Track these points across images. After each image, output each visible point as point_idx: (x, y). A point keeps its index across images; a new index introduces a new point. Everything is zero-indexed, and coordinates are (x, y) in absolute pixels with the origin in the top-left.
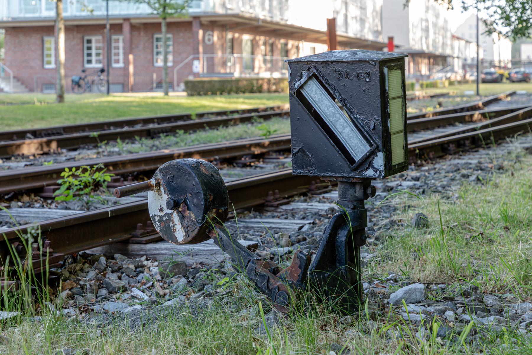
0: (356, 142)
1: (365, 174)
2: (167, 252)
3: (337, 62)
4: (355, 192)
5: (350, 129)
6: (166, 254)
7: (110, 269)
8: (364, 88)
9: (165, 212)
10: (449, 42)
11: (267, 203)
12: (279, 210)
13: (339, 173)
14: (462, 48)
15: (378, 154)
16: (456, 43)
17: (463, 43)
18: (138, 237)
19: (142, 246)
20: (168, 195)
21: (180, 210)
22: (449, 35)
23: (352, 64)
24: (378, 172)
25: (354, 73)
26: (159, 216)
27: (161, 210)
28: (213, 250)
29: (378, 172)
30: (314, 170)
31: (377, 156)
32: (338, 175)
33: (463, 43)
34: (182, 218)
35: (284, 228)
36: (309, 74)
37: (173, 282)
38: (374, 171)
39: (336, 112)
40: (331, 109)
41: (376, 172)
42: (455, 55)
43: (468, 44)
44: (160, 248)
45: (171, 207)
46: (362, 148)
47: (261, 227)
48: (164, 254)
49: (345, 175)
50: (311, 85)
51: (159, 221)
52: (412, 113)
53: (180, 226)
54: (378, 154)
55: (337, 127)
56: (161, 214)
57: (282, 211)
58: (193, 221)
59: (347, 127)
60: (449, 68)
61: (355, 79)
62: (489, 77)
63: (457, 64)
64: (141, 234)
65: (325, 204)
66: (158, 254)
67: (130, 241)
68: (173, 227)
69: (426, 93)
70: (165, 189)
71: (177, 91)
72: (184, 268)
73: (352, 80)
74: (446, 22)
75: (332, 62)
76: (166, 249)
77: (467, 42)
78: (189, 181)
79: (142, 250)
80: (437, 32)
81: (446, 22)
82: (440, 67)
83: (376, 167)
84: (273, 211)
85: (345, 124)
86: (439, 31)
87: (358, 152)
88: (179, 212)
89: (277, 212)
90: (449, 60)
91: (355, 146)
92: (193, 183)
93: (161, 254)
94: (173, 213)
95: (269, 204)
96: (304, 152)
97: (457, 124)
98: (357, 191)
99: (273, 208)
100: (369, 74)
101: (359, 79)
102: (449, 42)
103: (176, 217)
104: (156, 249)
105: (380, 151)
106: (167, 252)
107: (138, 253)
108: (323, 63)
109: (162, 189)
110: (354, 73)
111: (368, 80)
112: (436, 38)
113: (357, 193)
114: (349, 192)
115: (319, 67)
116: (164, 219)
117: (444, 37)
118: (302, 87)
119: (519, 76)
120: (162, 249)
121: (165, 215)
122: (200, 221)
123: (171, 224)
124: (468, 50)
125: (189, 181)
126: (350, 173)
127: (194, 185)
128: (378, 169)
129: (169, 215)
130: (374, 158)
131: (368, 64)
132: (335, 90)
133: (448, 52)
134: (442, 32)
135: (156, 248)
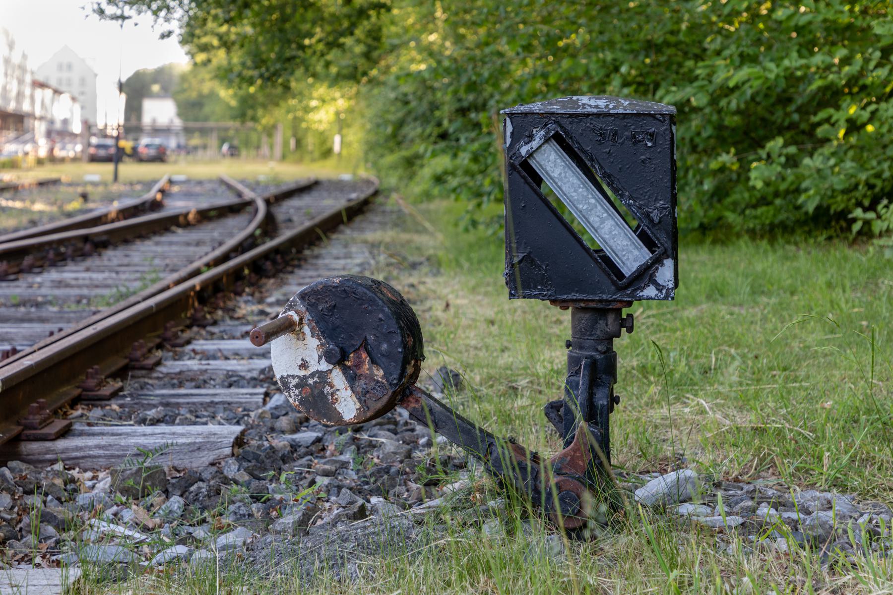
0: (625, 243)
1: (641, 294)
2: (101, 452)
3: (598, 115)
4: (607, 325)
5: (613, 223)
6: (99, 457)
7: (21, 489)
8: (643, 157)
9: (312, 369)
10: (28, 91)
11: (133, 363)
12: (155, 375)
13: (594, 294)
14: (48, 101)
15: (665, 261)
16: (39, 92)
17: (49, 93)
18: (35, 429)
19: (48, 444)
20: (320, 340)
21: (349, 363)
22: (28, 79)
23: (624, 118)
24: (664, 291)
25: (626, 133)
26: (298, 377)
27: (304, 365)
28: (195, 443)
29: (664, 291)
30: (548, 290)
31: (663, 265)
32: (591, 297)
33: (49, 93)
34: (352, 379)
35: (237, 403)
36: (547, 133)
37: (154, 503)
38: (657, 289)
39: (590, 196)
40: (580, 190)
41: (660, 291)
42: (38, 112)
43: (56, 96)
44: (86, 447)
45: (335, 360)
46: (636, 252)
47: (194, 403)
48: (95, 457)
49: (604, 297)
50: (547, 152)
51: (297, 386)
52: (175, 208)
53: (349, 392)
54: (665, 261)
55: (591, 219)
56: (302, 373)
57: (161, 375)
58: (378, 382)
59: (607, 219)
60: (28, 136)
61: (629, 143)
62: (102, 153)
63: (40, 128)
64: (40, 423)
65: (242, 362)
66: (83, 457)
67: (23, 437)
68: (332, 394)
69: (19, 177)
70: (312, 330)
71: (265, 159)
72: (162, 477)
73: (623, 143)
74: (24, 56)
75: (588, 115)
76: (99, 447)
77: (57, 92)
78: (370, 312)
79: (49, 451)
80: (9, 72)
81: (24, 56)
82: (12, 134)
83: (661, 282)
84: (144, 377)
85: (605, 215)
86: (13, 72)
87: (628, 259)
88: (345, 370)
89: (151, 378)
90: (28, 122)
91: (623, 250)
92: (381, 316)
93: (90, 457)
94: (331, 371)
95: (137, 364)
96: (533, 260)
97: (174, 228)
98: (609, 323)
99: (144, 372)
100: (652, 135)
101: (635, 143)
102: (28, 91)
103: (338, 378)
104: (78, 449)
105: (668, 257)
106: (101, 452)
107: (41, 457)
108: (571, 115)
109: (306, 329)
110: (626, 133)
111: (650, 144)
112: (7, 83)
113: (610, 326)
114: (598, 325)
115: (565, 122)
116: (311, 381)
117: (21, 82)
118: (531, 155)
119: (152, 152)
120: (90, 448)
121: (312, 375)
122: (395, 382)
123: (327, 390)
124: (56, 104)
125: (370, 312)
126: (614, 294)
127: (381, 320)
128: (664, 287)
129: (323, 376)
130: (657, 269)
131: (651, 119)
132: (592, 160)
133: (26, 107)
134: (17, 73)
135: (77, 447)
